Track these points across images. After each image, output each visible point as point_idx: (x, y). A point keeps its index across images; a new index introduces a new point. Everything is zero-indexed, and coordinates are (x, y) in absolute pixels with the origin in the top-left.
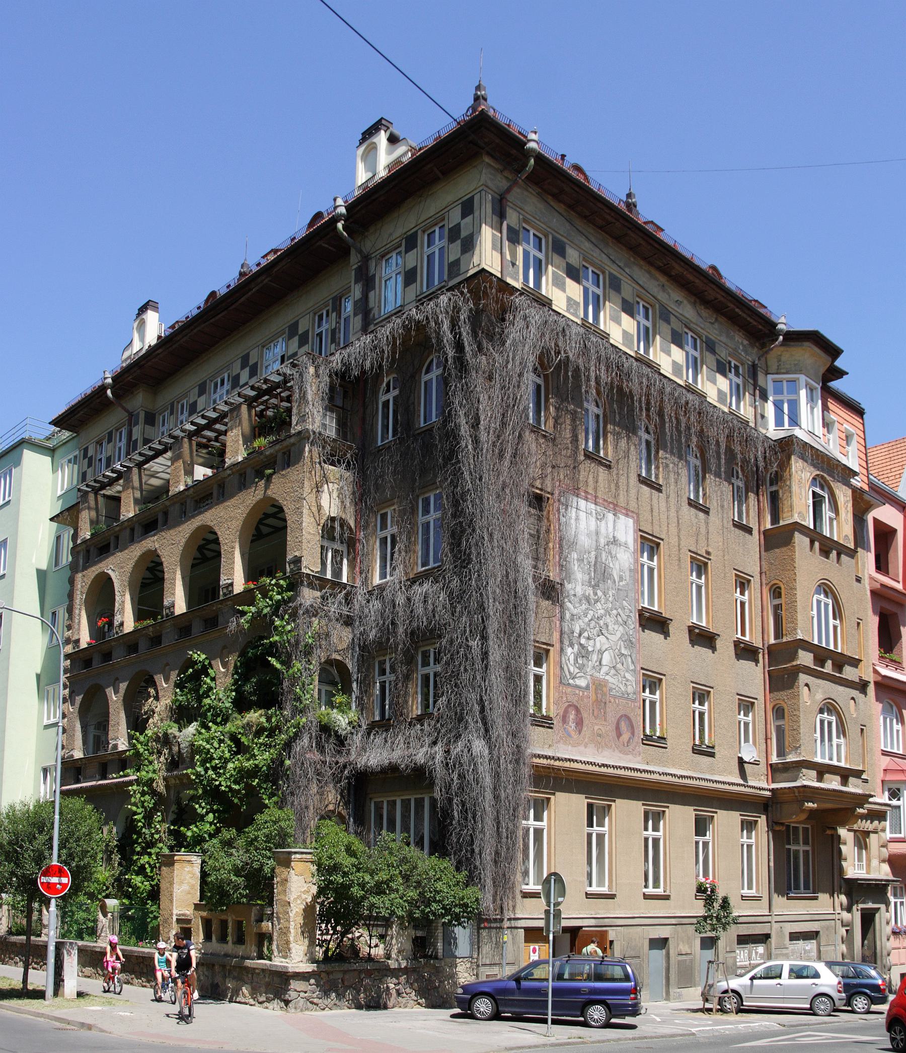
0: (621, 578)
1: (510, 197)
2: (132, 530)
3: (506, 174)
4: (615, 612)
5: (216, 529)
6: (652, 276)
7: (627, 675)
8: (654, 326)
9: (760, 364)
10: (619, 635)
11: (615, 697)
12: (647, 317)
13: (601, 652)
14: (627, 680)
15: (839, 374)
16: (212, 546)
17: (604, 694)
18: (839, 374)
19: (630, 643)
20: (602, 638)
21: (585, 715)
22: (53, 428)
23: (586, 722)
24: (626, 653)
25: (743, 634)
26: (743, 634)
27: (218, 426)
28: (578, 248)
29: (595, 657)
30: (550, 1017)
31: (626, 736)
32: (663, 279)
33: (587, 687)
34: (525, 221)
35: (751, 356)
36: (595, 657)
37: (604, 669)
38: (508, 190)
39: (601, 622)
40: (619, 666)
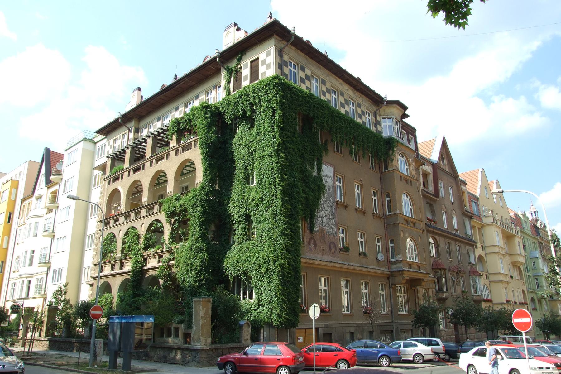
1: (285, 50)
2: (129, 172)
3: (283, 42)
5: (166, 171)
6: (337, 80)
8: (338, 97)
9: (378, 112)
10: (329, 211)
11: (328, 235)
12: (335, 94)
13: (322, 218)
15: (407, 116)
16: (163, 178)
17: (324, 234)
18: (407, 116)
19: (333, 214)
20: (322, 212)
21: (317, 242)
22: (96, 134)
23: (317, 245)
25: (376, 211)
26: (376, 211)
27: (162, 135)
28: (310, 69)
29: (320, 219)
30: (314, 367)
31: (333, 250)
32: (341, 81)
34: (290, 59)
35: (375, 109)
36: (320, 219)
37: (324, 224)
38: (284, 48)
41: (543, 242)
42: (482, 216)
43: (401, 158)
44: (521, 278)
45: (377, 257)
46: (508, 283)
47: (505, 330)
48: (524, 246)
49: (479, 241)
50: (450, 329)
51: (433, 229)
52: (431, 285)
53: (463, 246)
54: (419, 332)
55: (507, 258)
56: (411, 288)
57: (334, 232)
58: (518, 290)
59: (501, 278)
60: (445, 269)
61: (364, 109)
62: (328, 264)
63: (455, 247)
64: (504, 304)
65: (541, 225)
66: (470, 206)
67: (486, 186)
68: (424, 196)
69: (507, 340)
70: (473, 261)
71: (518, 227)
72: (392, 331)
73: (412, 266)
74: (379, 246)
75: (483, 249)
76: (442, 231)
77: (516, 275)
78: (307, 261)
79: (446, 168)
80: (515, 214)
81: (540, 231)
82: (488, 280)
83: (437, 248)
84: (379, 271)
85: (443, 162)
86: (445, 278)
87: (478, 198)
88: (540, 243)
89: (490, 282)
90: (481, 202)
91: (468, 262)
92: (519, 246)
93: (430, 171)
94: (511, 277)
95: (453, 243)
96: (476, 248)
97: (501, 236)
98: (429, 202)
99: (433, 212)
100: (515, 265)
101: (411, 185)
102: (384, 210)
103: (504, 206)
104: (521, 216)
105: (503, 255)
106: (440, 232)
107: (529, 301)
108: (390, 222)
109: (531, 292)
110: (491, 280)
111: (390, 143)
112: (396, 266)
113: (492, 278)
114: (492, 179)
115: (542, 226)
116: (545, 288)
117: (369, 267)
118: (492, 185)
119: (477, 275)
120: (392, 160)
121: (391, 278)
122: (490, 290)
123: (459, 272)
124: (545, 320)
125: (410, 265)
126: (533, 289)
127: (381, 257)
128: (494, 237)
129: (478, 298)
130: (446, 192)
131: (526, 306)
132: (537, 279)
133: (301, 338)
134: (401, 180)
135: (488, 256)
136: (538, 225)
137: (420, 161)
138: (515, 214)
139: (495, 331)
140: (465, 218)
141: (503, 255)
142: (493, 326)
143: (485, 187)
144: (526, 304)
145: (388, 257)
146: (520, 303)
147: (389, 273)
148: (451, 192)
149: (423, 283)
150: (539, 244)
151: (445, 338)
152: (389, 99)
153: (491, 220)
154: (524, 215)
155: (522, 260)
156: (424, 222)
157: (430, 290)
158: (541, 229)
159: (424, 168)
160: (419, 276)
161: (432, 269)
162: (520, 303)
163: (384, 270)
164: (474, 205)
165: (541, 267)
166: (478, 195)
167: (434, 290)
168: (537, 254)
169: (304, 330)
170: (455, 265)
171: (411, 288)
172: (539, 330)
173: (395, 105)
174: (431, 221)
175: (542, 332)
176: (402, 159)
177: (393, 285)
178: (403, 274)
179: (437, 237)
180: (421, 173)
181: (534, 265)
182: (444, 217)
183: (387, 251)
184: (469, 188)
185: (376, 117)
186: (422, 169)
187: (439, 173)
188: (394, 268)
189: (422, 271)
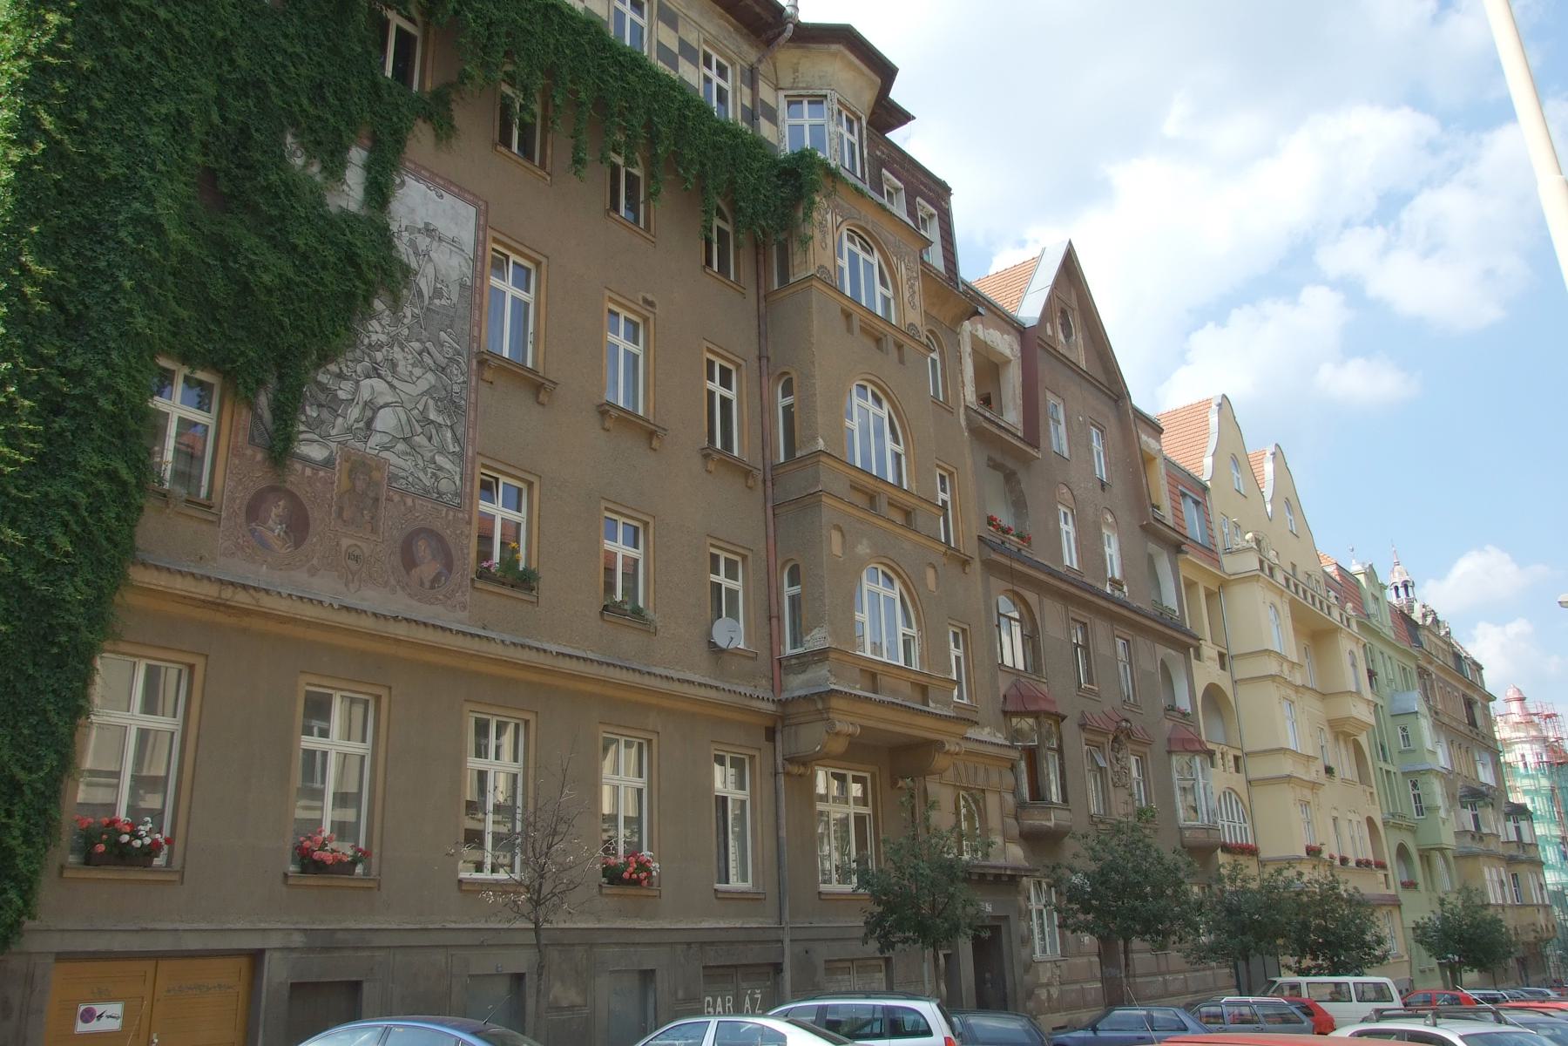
0: (437, 293)
4: (417, 345)
7: (439, 459)
9: (762, 68)
11: (404, 493)
14: (440, 469)
19: (450, 405)
24: (440, 420)
31: (428, 568)
33: (328, 463)
35: (752, 55)
36: (354, 413)
39: (379, 356)
40: (420, 440)
41: (1431, 668)
42: (1220, 549)
43: (857, 249)
44: (1363, 778)
45: (710, 634)
46: (1314, 786)
47: (1303, 956)
48: (1371, 674)
49: (1208, 636)
50: (1081, 954)
51: (1013, 563)
52: (995, 778)
53: (1141, 643)
54: (927, 968)
55: (1312, 705)
56: (894, 784)
57: (444, 485)
58: (1350, 816)
59: (1287, 766)
60: (1060, 718)
61: (692, 38)
62: (367, 623)
63: (1112, 646)
64: (1300, 859)
65: (1424, 616)
66: (1176, 510)
67: (1234, 455)
68: (977, 432)
69: (1305, 995)
70: (1183, 703)
71: (1349, 605)
72: (777, 968)
73: (883, 681)
74: (732, 594)
75: (1223, 667)
76: (1052, 573)
77: (1346, 767)
78: (208, 591)
79: (1081, 358)
80: (1339, 568)
81: (1423, 636)
82: (1242, 776)
83: (1032, 640)
84: (713, 694)
85: (1068, 336)
86: (1060, 750)
87: (1205, 489)
88: (1423, 673)
89: (1249, 782)
90: (1215, 502)
91: (1164, 702)
92: (1354, 665)
93: (1007, 352)
94: (1329, 770)
95: (1100, 628)
96: (1198, 657)
97: (1289, 622)
98: (998, 457)
99: (1019, 505)
100: (1342, 731)
101: (902, 361)
102: (766, 442)
103: (1302, 533)
104: (1361, 578)
105: (1296, 688)
106: (1042, 577)
107: (1389, 857)
108: (788, 487)
109: (1399, 827)
110: (1251, 776)
111: (800, 177)
112: (803, 677)
113: (1257, 769)
114: (1257, 443)
115: (1429, 620)
116: (1442, 813)
117: (657, 670)
118: (1261, 462)
119: (1196, 752)
120: (805, 242)
121: (780, 733)
122: (1249, 814)
123: (1121, 737)
124: (1444, 919)
125: (874, 676)
126: (1403, 817)
127: (732, 633)
128: (1263, 623)
129: (1202, 837)
130: (1079, 440)
131: (1380, 874)
132: (1415, 785)
133: (116, 1008)
134: (850, 330)
135: (1241, 689)
136: (1417, 615)
137: (957, 300)
138: (1339, 568)
139: (1256, 961)
140: (1153, 547)
141: (1296, 688)
142: (1249, 938)
143: (1235, 459)
144: (1381, 865)
145: (774, 640)
146: (1359, 863)
147: (769, 707)
148: (1097, 445)
149: (940, 761)
150: (1420, 676)
151: (1055, 992)
152: (808, 15)
153: (1251, 563)
154: (1371, 574)
155: (1363, 713)
156: (975, 533)
157: (992, 801)
158: (1424, 626)
159: (981, 332)
160: (921, 728)
161: (1005, 713)
162: (1359, 863)
163: (758, 695)
164: (1190, 512)
165: (1429, 745)
166: (1205, 477)
167: (1009, 798)
168: (1415, 700)
169: (148, 965)
170: (1107, 709)
171: (894, 784)
172: (1424, 954)
173: (834, 47)
174: (1007, 531)
175: (1434, 962)
176: (862, 255)
177: (790, 760)
178: (827, 710)
179: (1031, 597)
180: (967, 349)
181: (1406, 738)
182: (1067, 529)
183: (773, 617)
184: (1171, 446)
185: (753, 86)
186: (974, 337)
187: (1046, 369)
188: (797, 685)
189: (932, 707)
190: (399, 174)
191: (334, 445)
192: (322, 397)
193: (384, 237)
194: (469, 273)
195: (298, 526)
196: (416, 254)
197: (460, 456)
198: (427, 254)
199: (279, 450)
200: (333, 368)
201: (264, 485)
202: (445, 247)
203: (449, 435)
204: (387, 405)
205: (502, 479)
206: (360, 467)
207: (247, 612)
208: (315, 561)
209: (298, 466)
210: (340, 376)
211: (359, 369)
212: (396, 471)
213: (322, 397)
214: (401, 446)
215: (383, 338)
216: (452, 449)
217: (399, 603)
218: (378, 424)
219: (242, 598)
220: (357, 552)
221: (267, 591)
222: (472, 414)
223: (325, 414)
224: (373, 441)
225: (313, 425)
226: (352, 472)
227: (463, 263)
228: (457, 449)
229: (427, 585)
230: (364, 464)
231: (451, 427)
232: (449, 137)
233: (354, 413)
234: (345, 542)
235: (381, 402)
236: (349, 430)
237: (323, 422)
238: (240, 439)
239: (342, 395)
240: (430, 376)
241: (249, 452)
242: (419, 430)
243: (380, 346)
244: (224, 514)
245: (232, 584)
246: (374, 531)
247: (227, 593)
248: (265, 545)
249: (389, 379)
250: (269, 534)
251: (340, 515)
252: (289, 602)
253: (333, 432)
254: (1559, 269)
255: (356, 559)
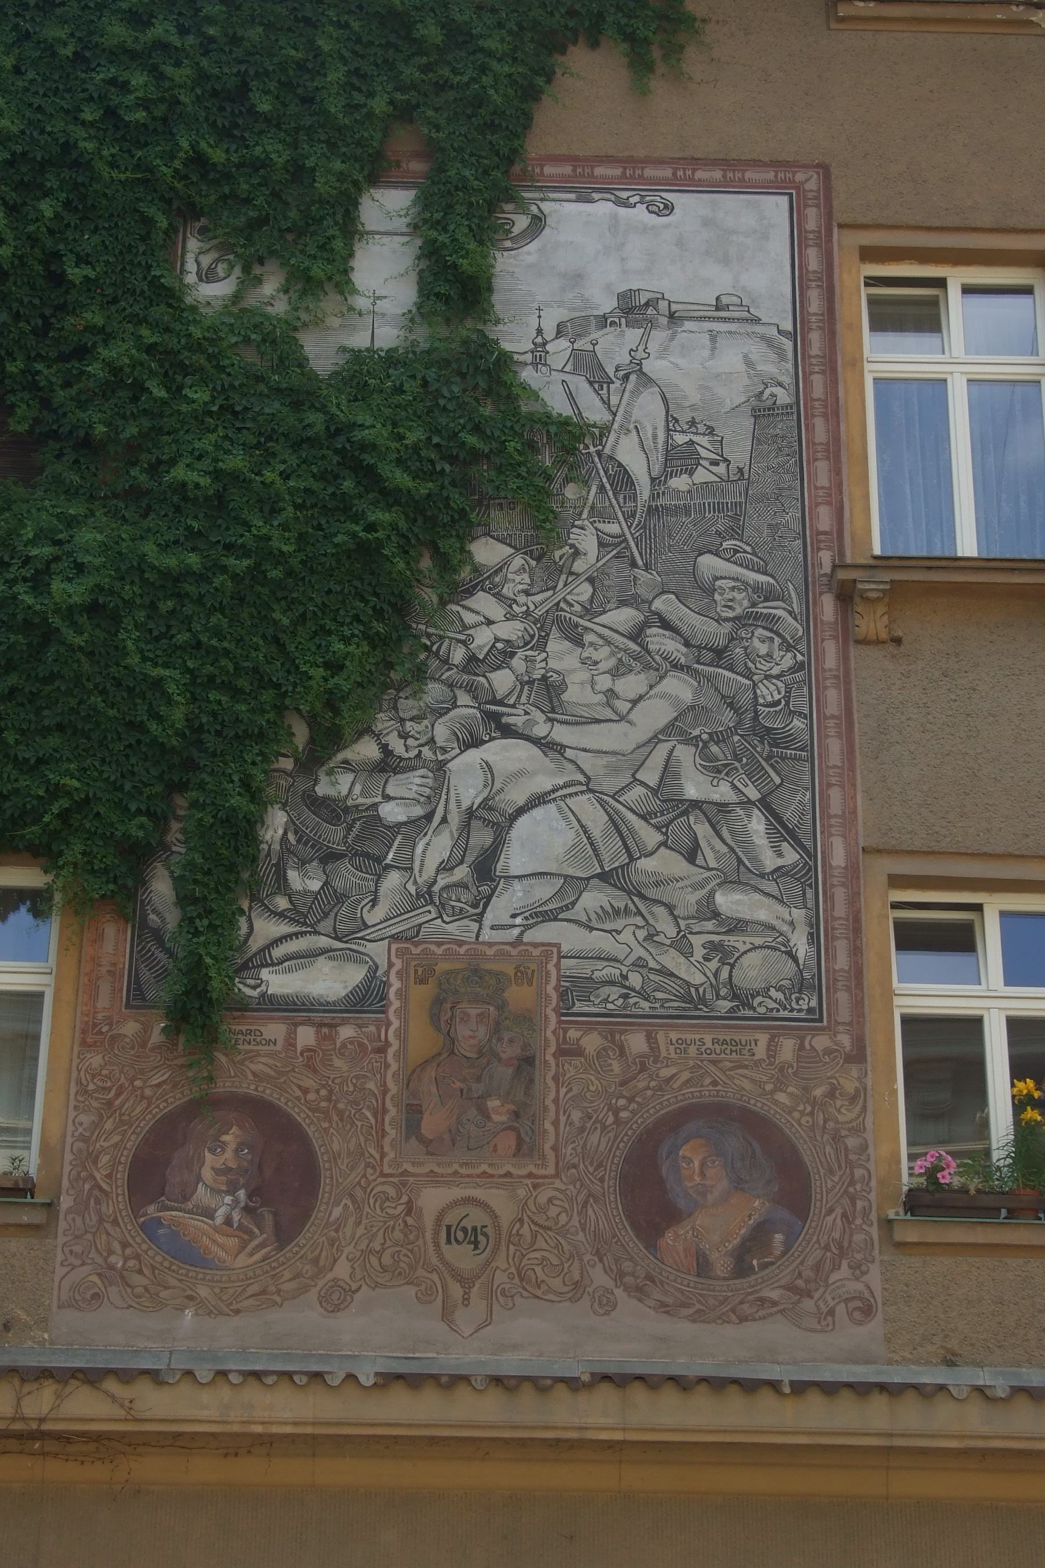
0: (679, 459)
4: (624, 617)
7: (727, 901)
11: (614, 1025)
14: (738, 926)
19: (755, 743)
24: (723, 792)
31: (719, 1214)
33: (367, 999)
36: (436, 848)
39: (502, 681)
40: (666, 863)
57: (753, 969)
190: (522, 207)
191: (378, 951)
192: (334, 836)
193: (492, 372)
194: (784, 372)
195: (285, 1184)
196: (599, 381)
197: (803, 878)
198: (636, 372)
199: (198, 1004)
200: (367, 750)
201: (176, 1099)
202: (694, 333)
203: (757, 825)
204: (539, 800)
205: (994, 905)
206: (460, 987)
207: (101, 1444)
208: (342, 1270)
209: (275, 1030)
210: (389, 764)
211: (441, 732)
212: (585, 968)
213: (334, 836)
214: (593, 899)
215: (510, 630)
216: (770, 861)
217: (634, 1334)
218: (516, 859)
219: (86, 1408)
220: (476, 1218)
221: (154, 1376)
222: (835, 746)
223: (347, 876)
224: (499, 910)
225: (303, 916)
226: (441, 1011)
227: (756, 350)
228: (791, 856)
229: (721, 1264)
230: (476, 973)
231: (765, 804)
232: (674, 51)
233: (436, 848)
234: (432, 1200)
235: (518, 796)
236: (426, 895)
237: (340, 898)
238: (103, 1002)
239: (392, 813)
240: (680, 688)
241: (130, 1028)
242: (650, 837)
243: (503, 654)
244: (66, 1202)
245: (46, 1374)
246: (525, 1147)
247: (40, 1402)
248: (189, 1255)
249: (541, 730)
250: (197, 1223)
251: (412, 1125)
252: (225, 1393)
253: (373, 917)
254: (918, 248)
255: (473, 1237)
